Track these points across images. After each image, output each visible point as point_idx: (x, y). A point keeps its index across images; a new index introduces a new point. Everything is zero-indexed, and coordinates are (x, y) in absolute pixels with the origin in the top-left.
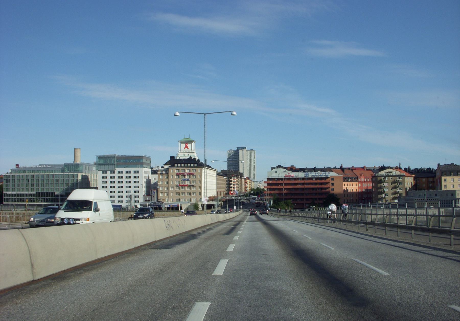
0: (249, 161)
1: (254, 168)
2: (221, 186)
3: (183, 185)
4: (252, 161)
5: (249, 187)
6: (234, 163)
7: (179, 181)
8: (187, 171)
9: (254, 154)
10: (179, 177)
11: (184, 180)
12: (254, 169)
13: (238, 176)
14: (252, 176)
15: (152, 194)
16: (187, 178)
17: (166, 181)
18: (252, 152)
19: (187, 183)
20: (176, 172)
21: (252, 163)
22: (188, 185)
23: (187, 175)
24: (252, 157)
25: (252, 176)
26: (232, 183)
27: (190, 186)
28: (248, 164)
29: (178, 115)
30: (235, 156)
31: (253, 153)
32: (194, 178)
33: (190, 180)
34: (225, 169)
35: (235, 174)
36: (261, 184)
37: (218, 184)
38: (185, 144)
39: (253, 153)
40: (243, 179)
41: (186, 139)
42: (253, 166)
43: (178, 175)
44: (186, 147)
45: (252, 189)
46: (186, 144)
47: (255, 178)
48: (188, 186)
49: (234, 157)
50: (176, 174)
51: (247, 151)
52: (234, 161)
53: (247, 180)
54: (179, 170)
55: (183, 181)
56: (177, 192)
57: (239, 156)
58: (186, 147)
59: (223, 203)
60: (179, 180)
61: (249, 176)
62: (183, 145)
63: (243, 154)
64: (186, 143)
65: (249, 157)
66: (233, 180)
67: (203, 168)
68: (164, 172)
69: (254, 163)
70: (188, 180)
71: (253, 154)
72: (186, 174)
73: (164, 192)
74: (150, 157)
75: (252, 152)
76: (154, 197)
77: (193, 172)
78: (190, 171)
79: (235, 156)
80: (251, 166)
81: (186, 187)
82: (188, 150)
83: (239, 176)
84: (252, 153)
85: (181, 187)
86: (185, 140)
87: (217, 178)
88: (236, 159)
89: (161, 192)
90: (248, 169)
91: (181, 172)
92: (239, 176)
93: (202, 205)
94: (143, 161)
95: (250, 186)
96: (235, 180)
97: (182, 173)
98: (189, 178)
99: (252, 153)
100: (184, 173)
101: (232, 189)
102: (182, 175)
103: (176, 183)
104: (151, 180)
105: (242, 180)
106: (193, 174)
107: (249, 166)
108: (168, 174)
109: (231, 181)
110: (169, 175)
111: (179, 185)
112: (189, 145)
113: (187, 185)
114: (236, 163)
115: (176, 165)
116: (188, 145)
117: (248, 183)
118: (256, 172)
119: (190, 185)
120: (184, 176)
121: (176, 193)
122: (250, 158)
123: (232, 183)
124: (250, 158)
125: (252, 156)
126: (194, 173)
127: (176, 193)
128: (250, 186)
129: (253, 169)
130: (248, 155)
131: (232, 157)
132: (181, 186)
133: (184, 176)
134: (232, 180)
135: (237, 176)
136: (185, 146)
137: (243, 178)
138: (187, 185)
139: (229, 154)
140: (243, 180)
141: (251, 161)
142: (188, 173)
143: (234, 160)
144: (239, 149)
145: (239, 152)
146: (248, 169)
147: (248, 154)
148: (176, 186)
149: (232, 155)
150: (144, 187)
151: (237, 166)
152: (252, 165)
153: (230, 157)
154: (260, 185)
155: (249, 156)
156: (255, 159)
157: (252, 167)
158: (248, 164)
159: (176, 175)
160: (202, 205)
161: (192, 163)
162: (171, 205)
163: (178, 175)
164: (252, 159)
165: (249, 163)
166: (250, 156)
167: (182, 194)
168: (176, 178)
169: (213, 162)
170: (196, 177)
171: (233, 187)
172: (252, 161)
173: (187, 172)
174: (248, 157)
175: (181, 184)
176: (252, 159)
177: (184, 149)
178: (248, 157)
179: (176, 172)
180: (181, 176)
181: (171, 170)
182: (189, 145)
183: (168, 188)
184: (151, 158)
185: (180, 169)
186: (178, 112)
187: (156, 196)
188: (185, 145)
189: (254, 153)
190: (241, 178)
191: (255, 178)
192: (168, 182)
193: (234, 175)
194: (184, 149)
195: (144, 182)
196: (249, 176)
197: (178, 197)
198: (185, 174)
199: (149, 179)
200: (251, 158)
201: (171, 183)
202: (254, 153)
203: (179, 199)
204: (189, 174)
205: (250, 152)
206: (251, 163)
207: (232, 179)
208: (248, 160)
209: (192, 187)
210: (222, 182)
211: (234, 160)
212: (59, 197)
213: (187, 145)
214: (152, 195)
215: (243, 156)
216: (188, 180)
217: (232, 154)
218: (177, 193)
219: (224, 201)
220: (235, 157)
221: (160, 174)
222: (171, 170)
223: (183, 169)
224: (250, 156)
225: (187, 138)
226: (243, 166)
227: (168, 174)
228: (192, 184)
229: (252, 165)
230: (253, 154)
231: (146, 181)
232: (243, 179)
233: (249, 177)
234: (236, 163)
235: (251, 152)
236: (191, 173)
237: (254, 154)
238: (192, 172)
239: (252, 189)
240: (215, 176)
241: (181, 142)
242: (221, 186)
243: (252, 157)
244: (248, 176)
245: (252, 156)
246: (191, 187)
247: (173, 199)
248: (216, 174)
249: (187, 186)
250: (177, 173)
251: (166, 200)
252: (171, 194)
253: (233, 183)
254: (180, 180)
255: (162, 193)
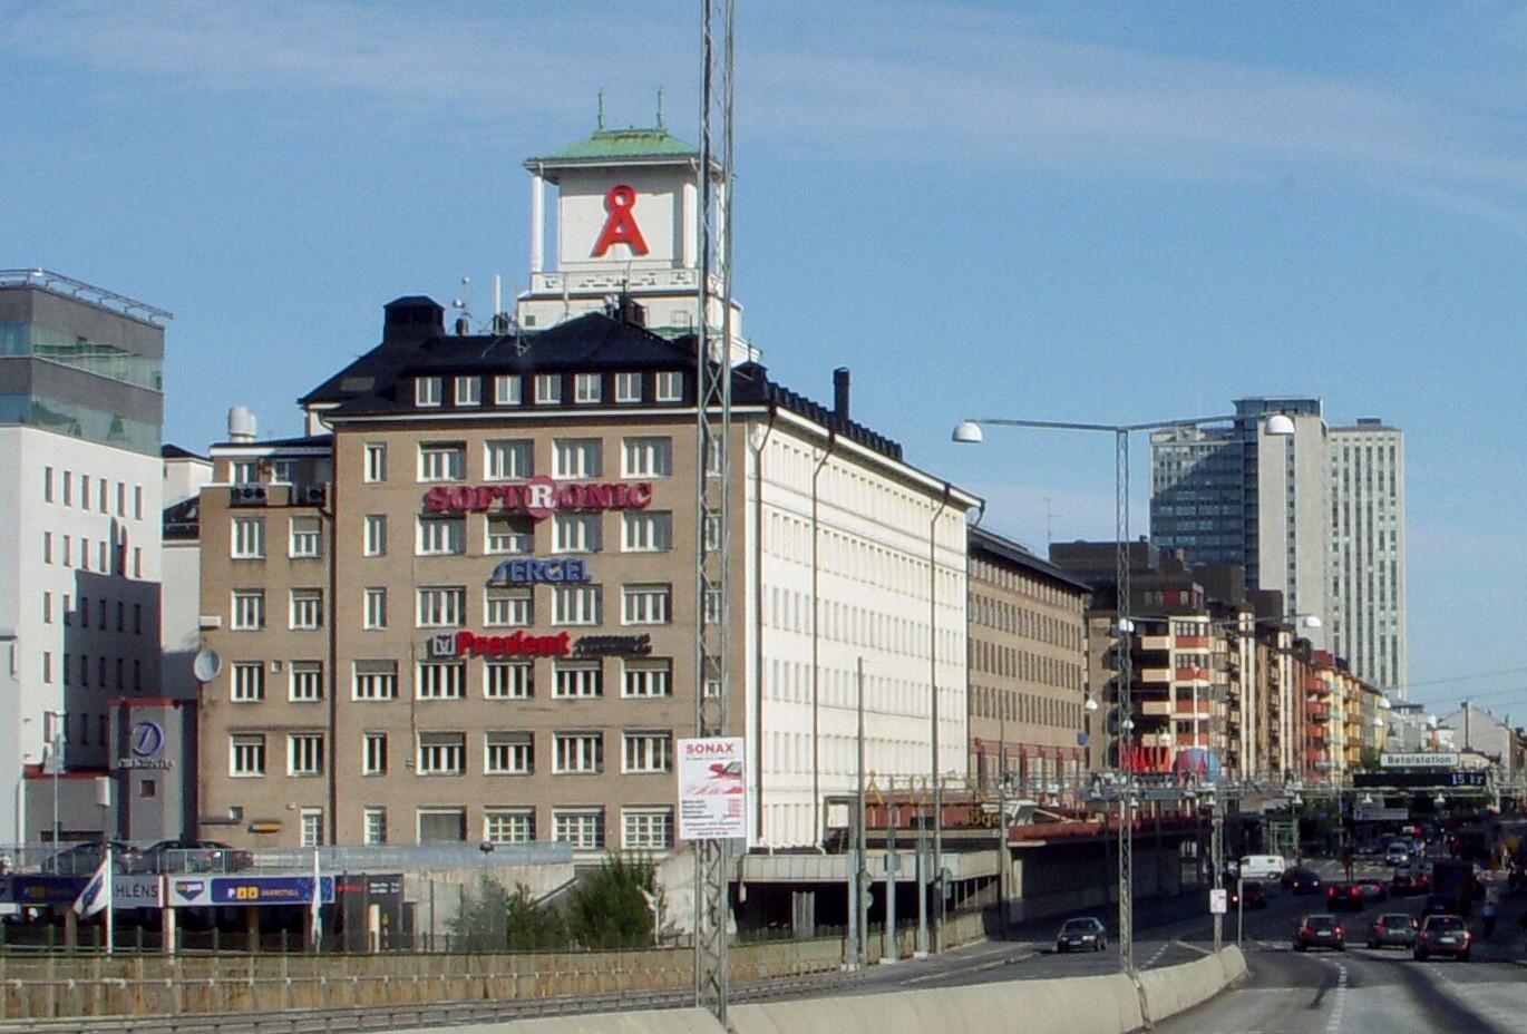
0: (1347, 524)
1: (1394, 583)
2: (1036, 689)
3: (503, 635)
4: (1370, 524)
5: (1343, 741)
6: (1216, 541)
7: (463, 592)
8: (561, 467)
9: (1392, 458)
10: (459, 548)
11: (519, 579)
12: (1394, 593)
13: (1234, 612)
14: (1371, 659)
15: (124, 752)
16: (555, 549)
17: (297, 591)
18: (1363, 446)
19: (555, 613)
20: (423, 471)
21: (1370, 539)
22: (574, 637)
23: (565, 510)
24: (1370, 489)
25: (1371, 659)
26: (1168, 675)
27: (597, 648)
28: (1336, 547)
29: (971, 438)
30: (1220, 480)
31: (1381, 449)
32: (651, 546)
33: (592, 570)
34: (1090, 539)
35: (1198, 588)
36: (1448, 734)
37: (979, 656)
38: (601, 198)
39: (1381, 449)
40: (1281, 658)
41: (619, 136)
42: (1382, 568)
43: (442, 509)
44: (621, 230)
45: (1369, 773)
46: (620, 201)
47: (1395, 674)
48: (570, 645)
49: (1214, 487)
50: (426, 498)
51: (1324, 428)
52: (1206, 525)
53: (1327, 675)
54: (461, 446)
55: (511, 585)
56: (432, 722)
57: (1251, 477)
58: (621, 230)
59: (1017, 868)
60: (458, 573)
61: (1343, 646)
62: (586, 212)
63: (1292, 458)
64: (623, 190)
65: (1346, 489)
66: (1182, 641)
67: (762, 429)
68: (274, 481)
69: (1388, 543)
70: (572, 576)
71: (1381, 458)
72: (548, 503)
73: (275, 729)
74: (156, 312)
75: (1363, 446)
76: (150, 788)
77: (637, 475)
78: (595, 465)
79: (1220, 480)
80: (1366, 569)
81: (548, 669)
82: (640, 262)
83: (1246, 620)
84: (1369, 450)
85: (481, 670)
86: (606, 148)
87: (979, 588)
88: (1225, 501)
89: (239, 734)
90: (1336, 592)
91: (487, 476)
92: (1246, 620)
93: (743, 895)
94: (21, 342)
95: (1356, 731)
96: (1202, 651)
97: (492, 491)
98: (581, 546)
99: (1369, 450)
100: (522, 492)
101: (1169, 707)
102: (493, 519)
103: (420, 618)
104: (163, 587)
105: (1275, 663)
106: (631, 502)
107: (1342, 569)
108: (320, 506)
109: (1160, 659)
110: (332, 517)
111: (465, 641)
112: (650, 210)
113: (564, 638)
114: (1226, 539)
115: (426, 392)
116: (636, 212)
117: (1330, 699)
118: (1405, 622)
119: (600, 633)
120: (522, 521)
121: (425, 737)
122: (1358, 494)
123: (1168, 675)
124: (1358, 494)
125: (1375, 477)
126: (645, 488)
127: (425, 737)
128: (1356, 731)
129: (1382, 598)
130: (1335, 474)
131: (1193, 488)
132: (490, 656)
133: (522, 521)
134: (1168, 643)
135: (1223, 611)
136: (604, 216)
137: (1283, 639)
138: (564, 638)
139: (1164, 462)
140: (1285, 663)
141: (1359, 525)
142: (573, 489)
143: (1209, 510)
144: (1249, 416)
145: (1252, 446)
146: (1336, 592)
147: (1335, 459)
148: (422, 653)
149: (1197, 472)
150: (31, 667)
151: (1239, 540)
152: (1370, 563)
153: (1178, 487)
154: (1443, 742)
155: (1346, 480)
156: (1400, 509)
157: (1371, 576)
158: (1336, 547)
159: (419, 508)
160: (743, 895)
161: (625, 368)
162: (236, 884)
163: (442, 509)
164: (1370, 509)
165: (1342, 540)
166: (1358, 479)
167: (499, 755)
168: (419, 550)
169: (973, 432)
170: (665, 539)
171: (1173, 693)
172: (1370, 524)
173: (555, 475)
174: (1335, 489)
175: (487, 619)
176: (1370, 509)
177: (600, 250)
178: (1335, 489)
179: (420, 478)
180: (479, 526)
181: (359, 456)
182: (650, 210)
183: (320, 676)
184: (161, 329)
185: (474, 432)
186: (974, 421)
187: (172, 785)
188: (610, 205)
189: (1387, 453)
190: (1265, 633)
191: (1395, 674)
192: (323, 604)
193: (1184, 596)
194: (600, 250)
195: (31, 607)
196: (1343, 646)
197: (451, 792)
198: (540, 498)
199: (130, 574)
200: (1364, 493)
201: (361, 615)
202: (1392, 449)
203: (463, 819)
204: (587, 504)
205: (1351, 445)
206: (1359, 539)
207: (1166, 633)
208: (1335, 510)
209: (617, 670)
210: (1038, 648)
211: (1209, 510)
212: (938, 836)
213: (631, 202)
214: (128, 762)
215: (1291, 473)
216: (572, 576)
217: (1192, 463)
218: (433, 742)
219: (1042, 843)
220: (1226, 487)
221: (227, 500)
222: (359, 456)
223: (506, 445)
224: (1358, 479)
225: (631, 134)
226: (1292, 566)
227: (320, 506)
228: (623, 622)
229: (1370, 563)
230: (1381, 458)
231: (71, 589)
232: (1285, 652)
233: (1343, 655)
234: (1226, 539)
235: (1363, 439)
236: (615, 489)
237: (1392, 458)
238: (624, 474)
239: (1369, 773)
240: (951, 570)
241: (563, 175)
242: (1036, 689)
243: (1370, 489)
244: (1337, 645)
245: (1375, 477)
246: (607, 660)
247: (383, 818)
248: (964, 548)
249: (553, 646)
250: (439, 491)
251: (304, 832)
252: (356, 757)
253: (1181, 673)
254: (475, 577)
255: (255, 747)
